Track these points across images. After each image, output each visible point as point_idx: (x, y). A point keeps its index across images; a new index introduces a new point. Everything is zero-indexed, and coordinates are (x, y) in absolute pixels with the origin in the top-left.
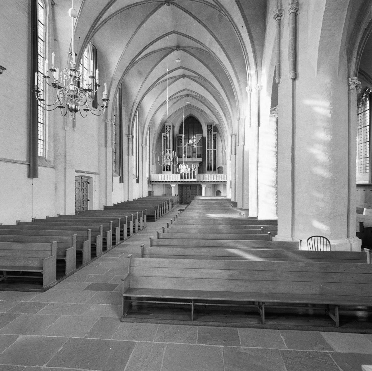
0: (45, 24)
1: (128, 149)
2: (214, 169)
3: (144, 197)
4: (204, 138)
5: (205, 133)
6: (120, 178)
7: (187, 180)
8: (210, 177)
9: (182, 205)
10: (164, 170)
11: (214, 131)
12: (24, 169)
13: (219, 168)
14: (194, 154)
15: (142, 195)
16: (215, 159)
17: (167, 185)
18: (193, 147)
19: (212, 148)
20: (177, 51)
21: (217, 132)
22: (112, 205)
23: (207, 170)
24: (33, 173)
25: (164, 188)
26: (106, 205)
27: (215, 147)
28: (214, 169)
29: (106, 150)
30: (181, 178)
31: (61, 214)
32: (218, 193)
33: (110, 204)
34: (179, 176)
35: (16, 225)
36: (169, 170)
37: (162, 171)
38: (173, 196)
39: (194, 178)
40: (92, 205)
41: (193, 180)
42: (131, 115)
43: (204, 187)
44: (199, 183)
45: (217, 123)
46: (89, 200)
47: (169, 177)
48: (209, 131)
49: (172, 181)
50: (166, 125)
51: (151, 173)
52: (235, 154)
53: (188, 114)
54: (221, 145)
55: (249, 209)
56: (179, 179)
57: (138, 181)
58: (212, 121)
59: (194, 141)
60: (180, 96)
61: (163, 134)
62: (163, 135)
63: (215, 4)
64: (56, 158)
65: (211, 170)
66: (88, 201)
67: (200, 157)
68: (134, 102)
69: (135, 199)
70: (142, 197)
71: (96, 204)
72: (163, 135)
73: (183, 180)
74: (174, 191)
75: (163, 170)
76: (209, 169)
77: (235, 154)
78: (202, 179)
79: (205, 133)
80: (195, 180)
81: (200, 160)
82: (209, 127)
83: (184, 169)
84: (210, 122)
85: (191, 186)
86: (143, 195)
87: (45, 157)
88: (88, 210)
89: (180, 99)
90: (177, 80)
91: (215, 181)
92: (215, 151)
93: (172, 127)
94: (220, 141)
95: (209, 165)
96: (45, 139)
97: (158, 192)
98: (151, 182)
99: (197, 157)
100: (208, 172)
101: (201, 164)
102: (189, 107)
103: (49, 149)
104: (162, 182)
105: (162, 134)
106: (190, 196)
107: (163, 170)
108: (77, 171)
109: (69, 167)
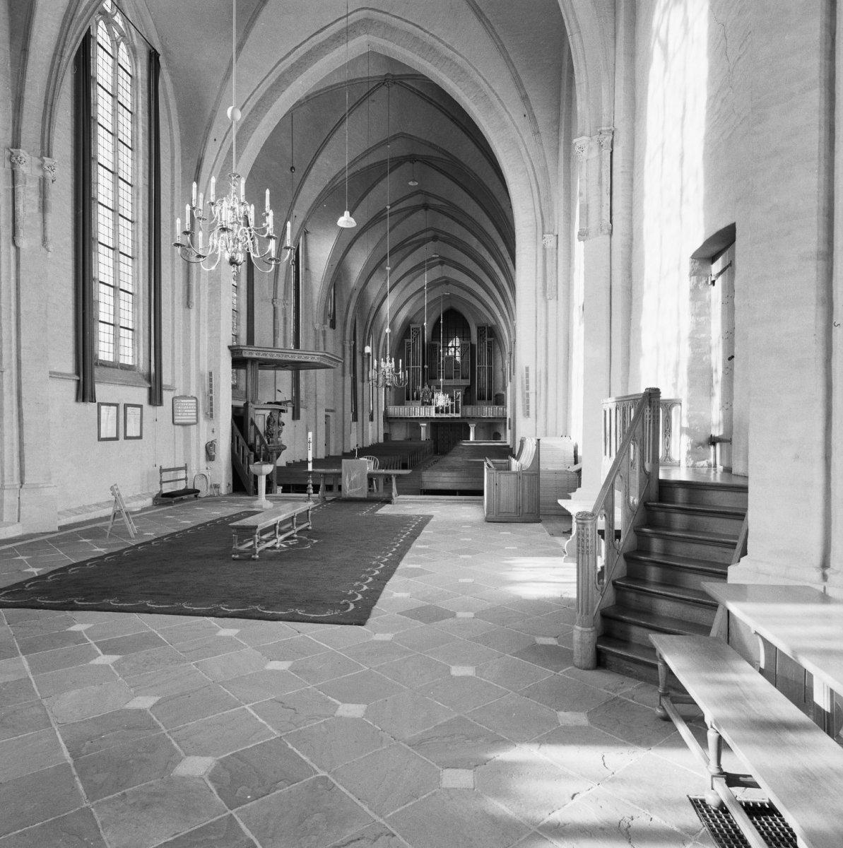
4: (473, 346)
5: (474, 339)
6: (150, 388)
7: (444, 415)
8: (488, 411)
9: (438, 455)
10: (408, 399)
11: (490, 336)
12: (70, 387)
13: (496, 395)
14: (457, 374)
15: (376, 439)
16: (490, 382)
17: (414, 423)
18: (455, 361)
20: (411, 164)
21: (492, 339)
22: (285, 465)
23: (478, 399)
24: (85, 393)
25: (407, 428)
27: (490, 363)
28: (490, 398)
29: (344, 379)
32: (497, 436)
38: (423, 441)
39: (457, 412)
41: (455, 415)
42: (367, 324)
44: (465, 421)
45: (494, 323)
48: (480, 335)
49: (421, 418)
50: (412, 326)
51: (388, 403)
53: (448, 306)
54: (501, 359)
56: (433, 415)
57: (372, 419)
58: (486, 322)
59: (454, 349)
60: (404, 209)
61: (407, 340)
65: (484, 399)
67: (467, 378)
68: (372, 307)
73: (439, 416)
74: (424, 434)
76: (481, 398)
78: (469, 414)
79: (474, 339)
80: (459, 415)
81: (467, 382)
82: (481, 330)
83: (441, 400)
84: (484, 321)
85: (451, 424)
89: (407, 216)
90: (412, 213)
91: (490, 418)
92: (490, 369)
93: (420, 329)
94: (499, 353)
96: (136, 329)
97: (399, 434)
98: (388, 419)
99: (462, 378)
100: (479, 402)
101: (468, 391)
102: (451, 297)
104: (406, 418)
106: (449, 442)
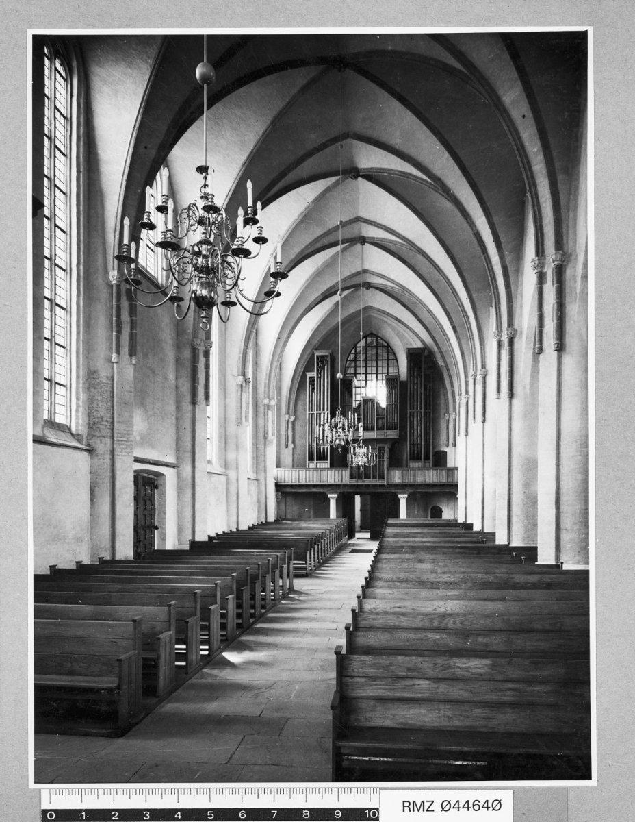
0: (69, 117)
1: (474, 395)
2: (427, 458)
3: (240, 528)
8: (428, 476)
19: (324, 410)
26: (113, 554)
30: (352, 477)
31: (60, 566)
33: (201, 537)
34: (346, 473)
35: (49, 573)
36: (324, 460)
37: (308, 462)
40: (163, 540)
43: (403, 499)
46: (157, 528)
47: (344, 476)
52: (484, 421)
55: (539, 546)
62: (309, 378)
63: (457, 65)
64: (92, 428)
66: (156, 530)
69: (213, 535)
70: (234, 530)
71: (170, 538)
72: (309, 378)
75: (309, 460)
76: (415, 457)
77: (484, 421)
86: (266, 518)
87: (68, 425)
88: (156, 549)
95: (415, 448)
103: (78, 406)
105: (306, 376)
107: (309, 460)
108: (137, 460)
109: (120, 448)
